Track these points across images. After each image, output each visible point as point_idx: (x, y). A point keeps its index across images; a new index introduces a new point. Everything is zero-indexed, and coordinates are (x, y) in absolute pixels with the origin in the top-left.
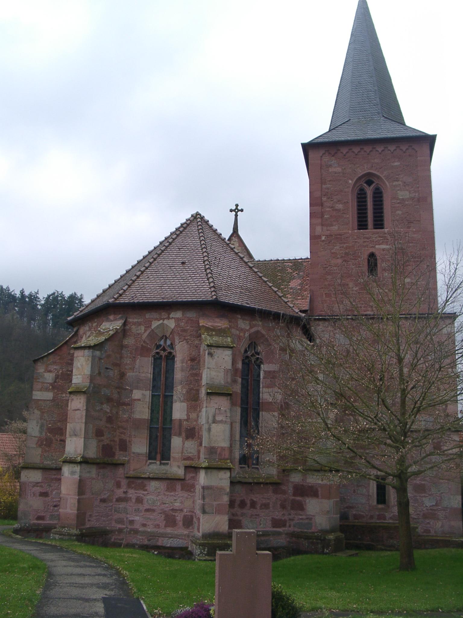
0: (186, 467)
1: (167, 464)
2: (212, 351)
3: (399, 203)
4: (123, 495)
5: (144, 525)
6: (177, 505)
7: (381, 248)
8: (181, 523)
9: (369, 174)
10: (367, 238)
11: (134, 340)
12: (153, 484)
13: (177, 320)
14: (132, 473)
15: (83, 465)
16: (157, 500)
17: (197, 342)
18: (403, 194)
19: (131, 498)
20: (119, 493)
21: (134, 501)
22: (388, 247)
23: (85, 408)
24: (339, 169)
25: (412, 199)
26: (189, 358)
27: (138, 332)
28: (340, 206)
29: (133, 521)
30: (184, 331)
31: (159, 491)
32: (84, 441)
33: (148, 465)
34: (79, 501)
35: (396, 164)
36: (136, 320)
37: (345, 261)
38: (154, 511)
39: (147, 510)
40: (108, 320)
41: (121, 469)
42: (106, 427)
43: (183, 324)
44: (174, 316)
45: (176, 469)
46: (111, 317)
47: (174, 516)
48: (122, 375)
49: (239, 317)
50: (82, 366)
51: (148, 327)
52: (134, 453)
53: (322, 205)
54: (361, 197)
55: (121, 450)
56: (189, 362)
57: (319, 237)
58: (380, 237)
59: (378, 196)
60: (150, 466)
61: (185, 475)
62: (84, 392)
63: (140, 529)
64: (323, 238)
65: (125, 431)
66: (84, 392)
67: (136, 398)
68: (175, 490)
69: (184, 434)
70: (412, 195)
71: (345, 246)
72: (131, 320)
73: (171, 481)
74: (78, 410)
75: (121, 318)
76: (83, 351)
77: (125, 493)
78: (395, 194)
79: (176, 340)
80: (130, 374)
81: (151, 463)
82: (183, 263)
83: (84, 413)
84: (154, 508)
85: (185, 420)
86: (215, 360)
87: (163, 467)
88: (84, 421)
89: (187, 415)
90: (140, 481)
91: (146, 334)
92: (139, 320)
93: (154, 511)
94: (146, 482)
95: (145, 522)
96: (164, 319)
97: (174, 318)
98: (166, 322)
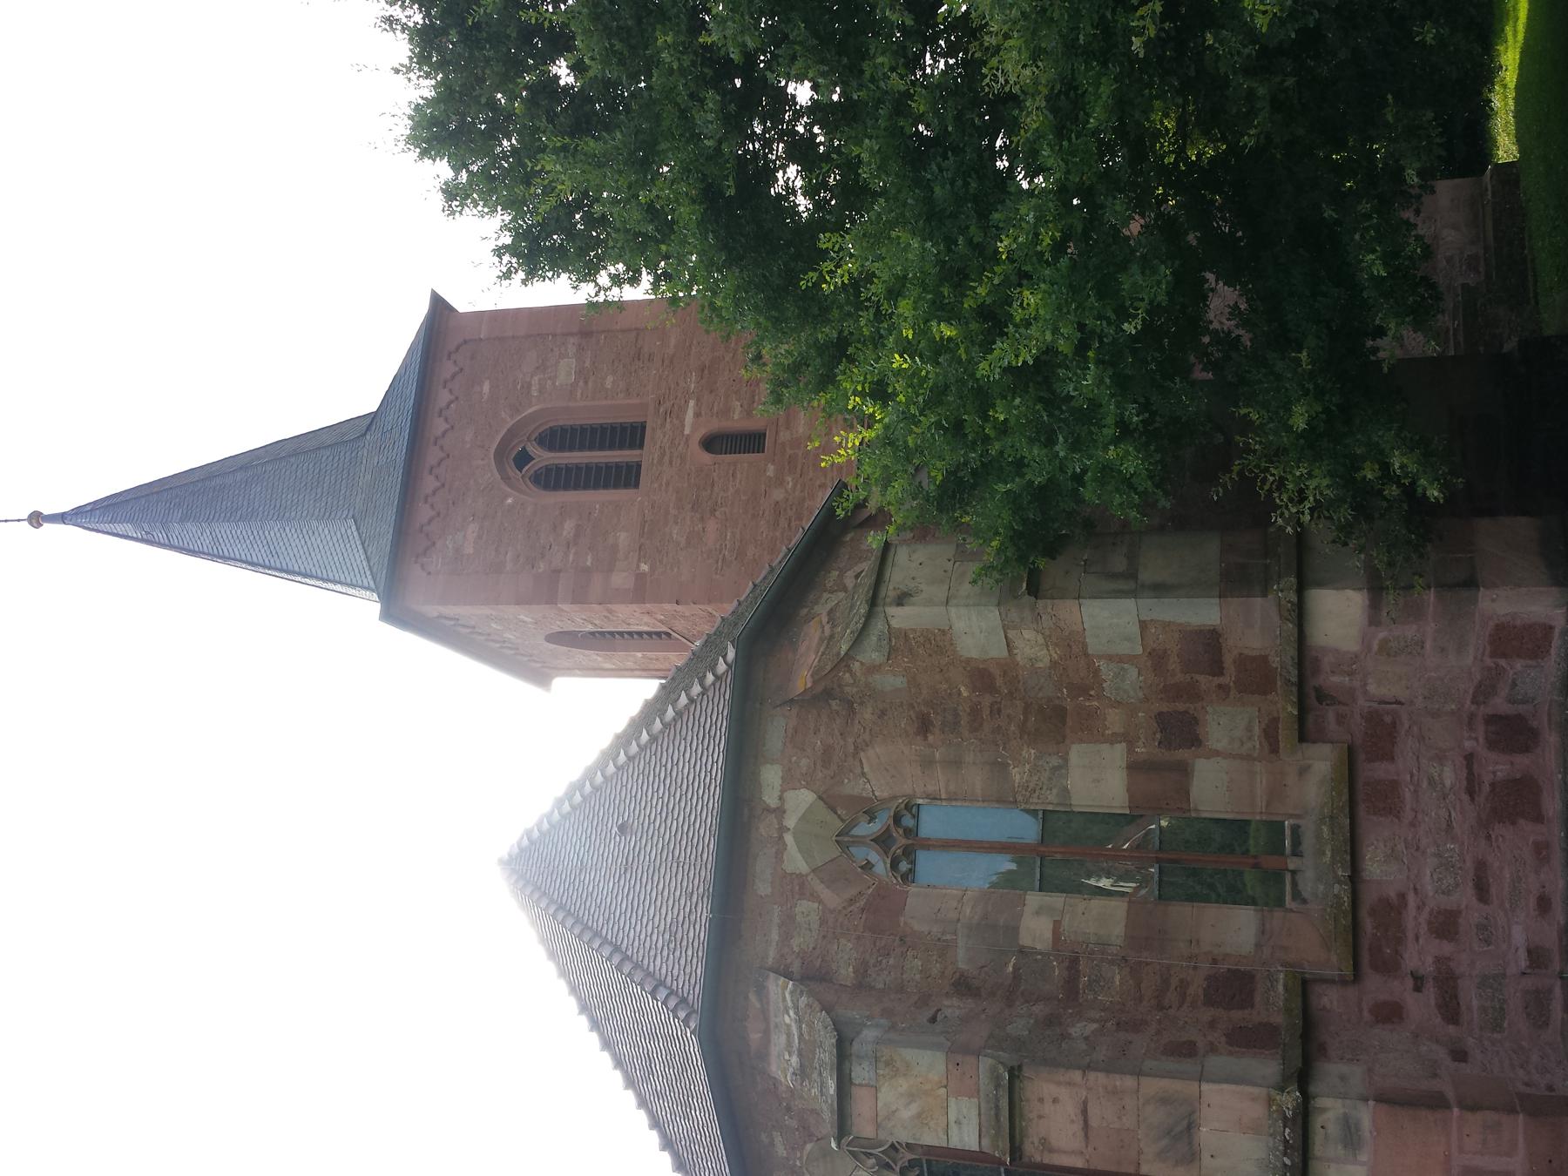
0: (1302, 738)
1: (1295, 830)
2: (892, 594)
3: (586, 383)
4: (1430, 993)
5: (1544, 904)
6: (1449, 776)
8: (1522, 761)
10: (663, 455)
11: (843, 941)
12: (1375, 867)
13: (789, 782)
14: (1334, 961)
15: (1312, 1089)
16: (1438, 855)
17: (867, 714)
18: (566, 371)
19: (1438, 960)
20: (1421, 1006)
21: (1447, 948)
22: (692, 403)
23: (1077, 1076)
27: (815, 926)
28: (569, 527)
29: (1529, 952)
30: (827, 756)
31: (1401, 847)
32: (1214, 1081)
33: (1304, 901)
34: (1471, 1106)
35: (486, 387)
36: (775, 936)
37: (713, 511)
38: (1481, 867)
39: (1482, 891)
40: (763, 1055)
41: (1325, 1001)
42: (1158, 1032)
44: (776, 793)
45: (1313, 777)
46: (755, 1037)
47: (1493, 785)
48: (963, 986)
49: (805, 611)
50: (911, 1097)
51: (802, 885)
52: (1258, 946)
53: (557, 571)
54: (552, 479)
55: (1247, 1002)
56: (931, 738)
57: (640, 577)
58: (663, 425)
59: (555, 438)
60: (1305, 895)
62: (1015, 1073)
63: (1561, 919)
64: (645, 567)
65: (1174, 982)
66: (1015, 1073)
67: (1048, 935)
68: (1394, 785)
69: (1182, 754)
70: (572, 350)
71: (673, 511)
72: (772, 953)
73: (1360, 799)
74: (1085, 1112)
75: (761, 990)
76: (854, 1090)
77: (1419, 983)
78: (563, 389)
79: (856, 792)
80: (962, 959)
81: (1297, 895)
82: (622, 829)
83: (1098, 1079)
84: (1469, 864)
85: (1130, 751)
86: (922, 587)
88: (1129, 1082)
90: (1368, 924)
91: (826, 894)
92: (776, 920)
93: (1481, 867)
94: (1369, 898)
95: (1532, 902)
96: (782, 829)
97: (782, 791)
98: (791, 822)
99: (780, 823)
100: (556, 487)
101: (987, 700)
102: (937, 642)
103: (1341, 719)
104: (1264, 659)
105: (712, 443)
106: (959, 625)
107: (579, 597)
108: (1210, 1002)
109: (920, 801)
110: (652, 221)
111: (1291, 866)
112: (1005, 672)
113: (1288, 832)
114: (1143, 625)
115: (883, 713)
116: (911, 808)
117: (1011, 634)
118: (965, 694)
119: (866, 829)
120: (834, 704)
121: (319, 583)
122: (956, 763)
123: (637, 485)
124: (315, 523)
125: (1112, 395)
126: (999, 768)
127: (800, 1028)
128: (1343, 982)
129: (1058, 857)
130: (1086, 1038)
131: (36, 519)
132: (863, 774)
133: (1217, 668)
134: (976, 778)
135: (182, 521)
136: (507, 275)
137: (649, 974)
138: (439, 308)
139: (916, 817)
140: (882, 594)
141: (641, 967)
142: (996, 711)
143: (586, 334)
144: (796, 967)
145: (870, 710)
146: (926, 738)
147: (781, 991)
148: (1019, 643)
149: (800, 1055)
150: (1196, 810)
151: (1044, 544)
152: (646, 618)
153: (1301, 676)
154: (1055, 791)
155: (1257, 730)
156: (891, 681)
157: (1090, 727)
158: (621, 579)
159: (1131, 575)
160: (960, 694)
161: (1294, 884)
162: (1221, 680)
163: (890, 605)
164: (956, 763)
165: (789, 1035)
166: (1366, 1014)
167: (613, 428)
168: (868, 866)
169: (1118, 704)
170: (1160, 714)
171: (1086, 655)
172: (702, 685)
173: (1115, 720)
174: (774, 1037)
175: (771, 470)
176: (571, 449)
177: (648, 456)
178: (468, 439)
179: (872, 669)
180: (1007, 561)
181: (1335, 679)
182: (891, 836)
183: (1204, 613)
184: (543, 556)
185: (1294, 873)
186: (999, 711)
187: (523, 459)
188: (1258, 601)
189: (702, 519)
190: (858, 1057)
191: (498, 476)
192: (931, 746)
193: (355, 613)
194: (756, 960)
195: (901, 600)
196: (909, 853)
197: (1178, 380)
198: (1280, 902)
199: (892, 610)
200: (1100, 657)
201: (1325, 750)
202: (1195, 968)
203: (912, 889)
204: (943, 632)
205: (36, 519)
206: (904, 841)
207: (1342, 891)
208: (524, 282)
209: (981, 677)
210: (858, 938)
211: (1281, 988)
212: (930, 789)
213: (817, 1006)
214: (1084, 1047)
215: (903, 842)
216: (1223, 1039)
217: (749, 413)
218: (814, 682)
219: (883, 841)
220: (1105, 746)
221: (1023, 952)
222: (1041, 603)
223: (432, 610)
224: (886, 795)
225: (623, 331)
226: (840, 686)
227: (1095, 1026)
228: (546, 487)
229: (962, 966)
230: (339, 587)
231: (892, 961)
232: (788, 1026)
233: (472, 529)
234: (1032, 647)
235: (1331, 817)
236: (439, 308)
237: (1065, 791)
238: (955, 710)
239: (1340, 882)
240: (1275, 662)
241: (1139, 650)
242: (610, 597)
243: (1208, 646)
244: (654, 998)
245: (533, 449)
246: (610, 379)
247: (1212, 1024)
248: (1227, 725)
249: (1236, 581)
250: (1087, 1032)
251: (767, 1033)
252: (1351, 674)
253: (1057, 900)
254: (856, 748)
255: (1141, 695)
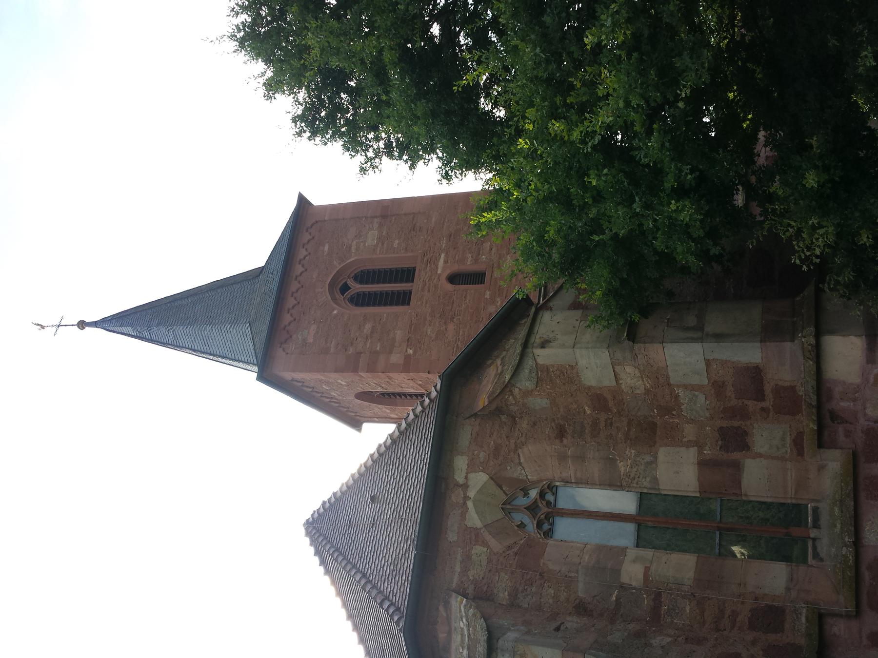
0: (821, 445)
1: (816, 510)
2: (538, 341)
3: (383, 244)
7: (443, 267)
9: (332, 286)
11: (502, 574)
13: (472, 467)
17: (524, 425)
18: (371, 238)
22: (443, 256)
24: (314, 327)
25: (381, 225)
26: (558, 441)
27: (484, 563)
28: (368, 327)
30: (496, 452)
33: (822, 560)
36: (458, 568)
41: (835, 629)
43: (482, 455)
44: (464, 475)
45: (828, 473)
46: (442, 636)
48: (582, 609)
49: (490, 361)
51: (477, 536)
52: (788, 589)
54: (361, 300)
56: (565, 441)
58: (426, 268)
59: (365, 277)
60: (822, 555)
61: (841, 448)
64: (410, 351)
69: (736, 456)
70: (376, 225)
71: (429, 318)
72: (456, 579)
75: (447, 605)
78: (370, 249)
79: (515, 475)
80: (582, 590)
81: (816, 555)
82: (373, 499)
85: (700, 452)
87: (824, 520)
89: (688, 447)
90: (866, 575)
91: (493, 542)
92: (459, 558)
96: (466, 498)
97: (467, 473)
98: (472, 494)
99: (465, 494)
100: (362, 305)
101: (603, 417)
102: (568, 375)
103: (848, 434)
104: (793, 389)
105: (453, 279)
106: (582, 363)
107: (371, 369)
108: (752, 627)
109: (558, 484)
110: (380, 85)
111: (812, 535)
112: (614, 397)
113: (810, 512)
114: (708, 363)
115: (535, 424)
116: (552, 488)
117: (618, 368)
118: (589, 412)
119: (522, 501)
120: (503, 418)
121: (231, 362)
122: (581, 458)
123: (408, 304)
124: (228, 326)
125: (672, 159)
126: (610, 462)
127: (469, 630)
128: (848, 616)
129: (650, 524)
130: (663, 647)
131: (82, 325)
132: (520, 464)
133: (760, 395)
134: (594, 468)
135: (158, 325)
136: (299, 134)
137: (380, 592)
138: (303, 202)
139: (555, 494)
140: (532, 341)
141: (376, 588)
142: (609, 424)
143: (384, 216)
144: (470, 590)
145: (526, 422)
146: (562, 441)
147: (458, 605)
148: (623, 376)
149: (469, 649)
150: (746, 495)
151: (639, 301)
152: (412, 384)
153: (819, 401)
154: (648, 479)
155: (788, 440)
156: (539, 402)
157: (673, 437)
158: (396, 358)
159: (700, 328)
160: (585, 412)
161: (815, 548)
162: (764, 404)
163: (537, 347)
164: (581, 458)
165: (462, 635)
166: (865, 641)
167: (397, 270)
168: (522, 526)
169: (692, 421)
170: (721, 428)
171: (669, 385)
172: (422, 405)
173: (689, 432)
174: (454, 636)
175: (488, 295)
176: (372, 283)
177: (416, 286)
178: (314, 277)
179: (527, 393)
180: (612, 314)
181: (843, 404)
182: (538, 506)
183: (750, 354)
184: (352, 344)
185: (814, 540)
186: (611, 424)
187: (345, 288)
188: (788, 345)
189: (445, 323)
190: (502, 650)
191: (329, 298)
192: (565, 446)
193: (244, 379)
194: (414, 565)
195: (543, 345)
196: (548, 516)
197: (721, 151)
198: (805, 561)
199: (538, 352)
200: (678, 386)
201: (836, 454)
202: (743, 603)
203: (550, 542)
204: (572, 367)
205: (82, 325)
206: (545, 510)
207: (848, 552)
208: (310, 138)
209: (599, 400)
210: (512, 573)
211: (803, 620)
212: (564, 475)
213: (479, 615)
214: (660, 652)
215: (546, 513)
216: (761, 652)
217: (476, 261)
218: (490, 402)
219: (532, 509)
220: (683, 449)
221: (622, 587)
222: (636, 346)
223: (288, 375)
224: (535, 478)
225: (405, 214)
226: (507, 405)
227: (670, 639)
228: (357, 305)
229: (580, 594)
230: (241, 365)
231: (534, 589)
232: (462, 629)
233: (314, 327)
234: (631, 378)
235: (841, 501)
236: (303, 202)
237: (655, 480)
238: (582, 422)
239: (846, 546)
240: (801, 391)
241: (706, 382)
242: (390, 368)
243: (754, 376)
244: (376, 601)
245: (351, 283)
246: (397, 242)
247: (754, 643)
248: (768, 436)
249: (772, 332)
250: (664, 643)
251: (449, 633)
252: (855, 400)
253: (648, 553)
254: (516, 446)
255: (708, 415)
